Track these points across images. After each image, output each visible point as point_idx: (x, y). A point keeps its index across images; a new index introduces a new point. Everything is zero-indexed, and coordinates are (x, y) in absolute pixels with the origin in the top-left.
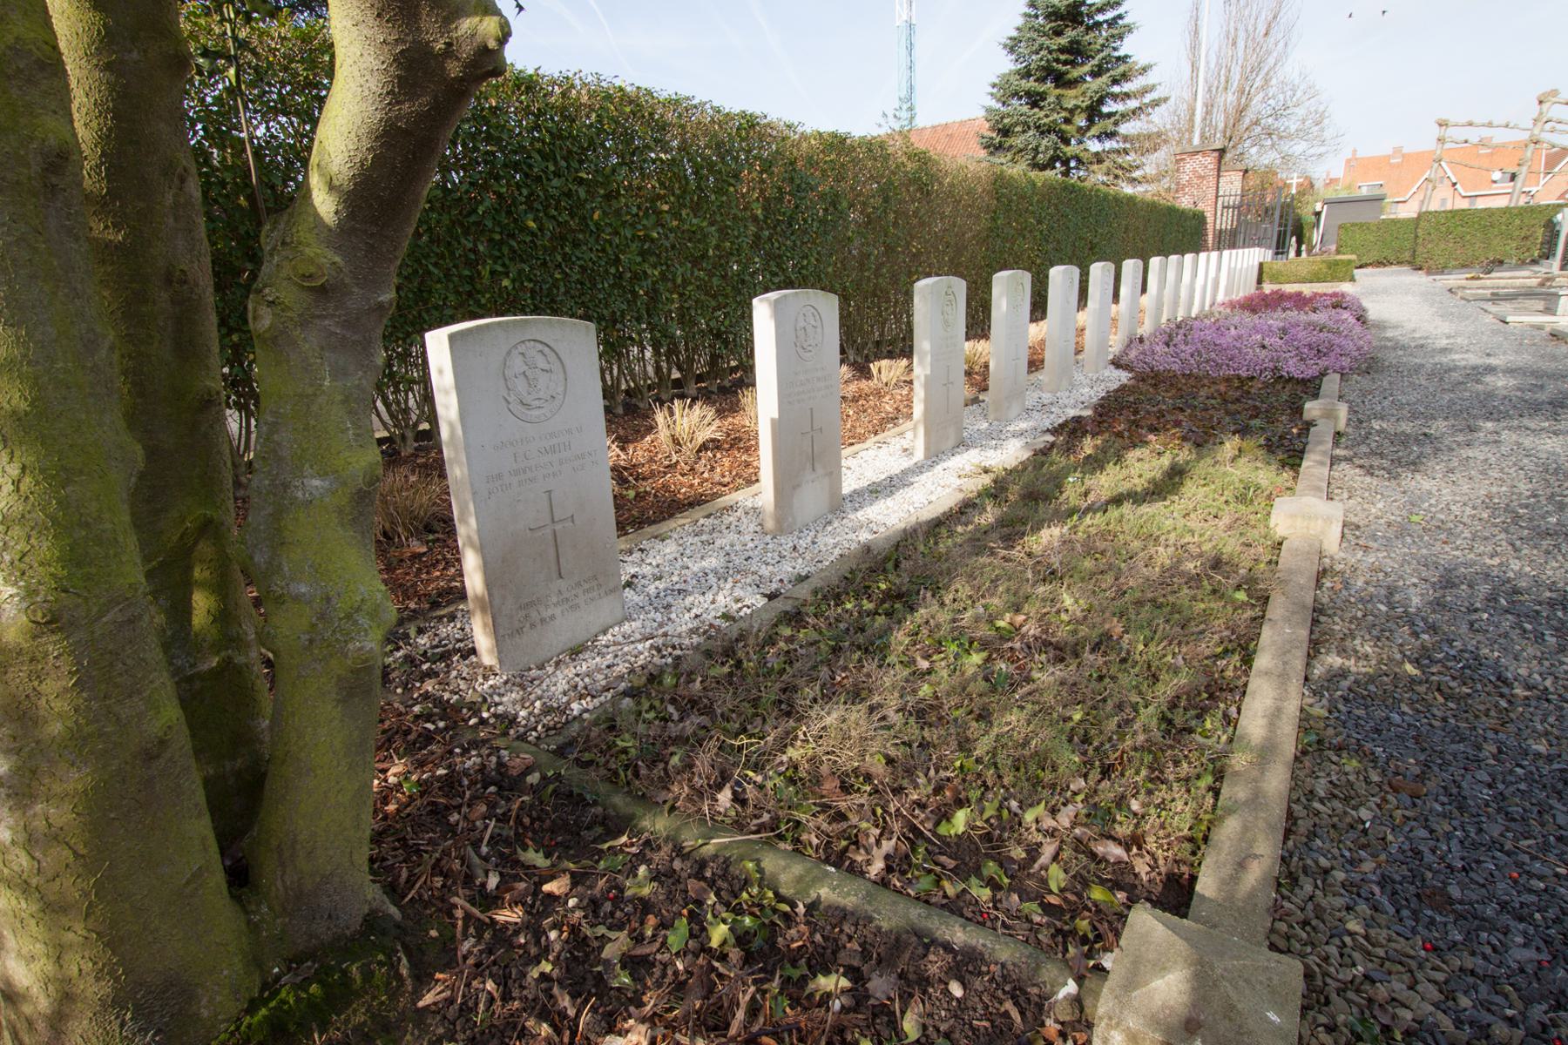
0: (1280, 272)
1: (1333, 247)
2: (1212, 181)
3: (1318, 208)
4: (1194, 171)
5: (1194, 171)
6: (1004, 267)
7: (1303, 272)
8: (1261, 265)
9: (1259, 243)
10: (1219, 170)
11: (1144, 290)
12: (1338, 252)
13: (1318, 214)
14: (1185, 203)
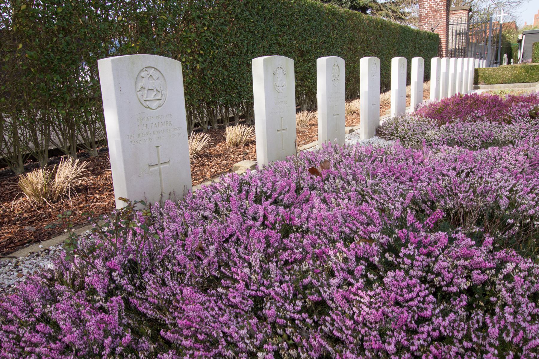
0: (490, 76)
1: (530, 60)
2: (443, 14)
3: (520, 38)
4: (431, 7)
5: (431, 7)
6: (323, 55)
7: (508, 74)
8: (476, 71)
9: (480, 56)
10: (448, 11)
11: (409, 82)
12: (533, 61)
13: (520, 41)
14: (426, 28)
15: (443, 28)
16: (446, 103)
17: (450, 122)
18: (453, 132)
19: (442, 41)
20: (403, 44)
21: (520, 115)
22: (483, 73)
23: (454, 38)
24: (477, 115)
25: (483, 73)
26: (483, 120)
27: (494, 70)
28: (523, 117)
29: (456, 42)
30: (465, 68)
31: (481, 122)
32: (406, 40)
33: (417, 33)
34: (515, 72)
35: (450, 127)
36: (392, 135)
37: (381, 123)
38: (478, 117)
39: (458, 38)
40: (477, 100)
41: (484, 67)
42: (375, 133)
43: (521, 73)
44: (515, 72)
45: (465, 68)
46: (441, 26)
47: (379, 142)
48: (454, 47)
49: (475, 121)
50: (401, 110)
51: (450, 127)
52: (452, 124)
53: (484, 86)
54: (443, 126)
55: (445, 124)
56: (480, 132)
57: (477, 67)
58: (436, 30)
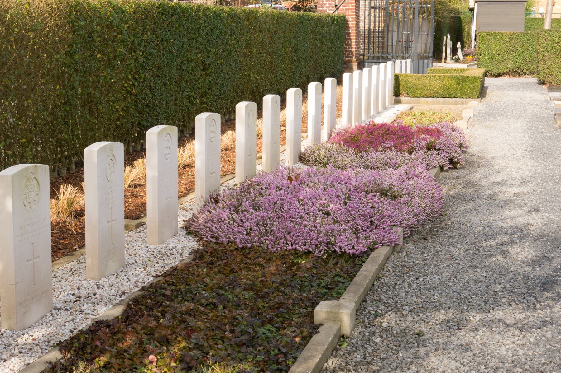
8: (397, 78)
13: (472, 10)
15: (352, 6)
16: (360, 130)
17: (365, 151)
18: (368, 160)
19: (351, 26)
20: (301, 39)
21: (420, 147)
22: (406, 82)
23: (367, 13)
24: (387, 146)
25: (406, 82)
26: (391, 150)
27: (419, 78)
28: (421, 148)
29: (370, 20)
30: (382, 78)
31: (389, 152)
32: (305, 32)
33: (318, 19)
34: (444, 82)
35: (365, 156)
36: (315, 162)
37: (303, 150)
38: (388, 148)
39: (372, 14)
40: (388, 130)
41: (408, 72)
42: (298, 160)
43: (451, 85)
44: (444, 82)
45: (382, 78)
46: (348, 3)
47: (302, 168)
48: (367, 28)
49: (385, 151)
50: (317, 137)
51: (365, 156)
52: (367, 153)
53: (407, 99)
54: (360, 154)
55: (361, 152)
56: (389, 161)
57: (397, 72)
58: (341, 7)
